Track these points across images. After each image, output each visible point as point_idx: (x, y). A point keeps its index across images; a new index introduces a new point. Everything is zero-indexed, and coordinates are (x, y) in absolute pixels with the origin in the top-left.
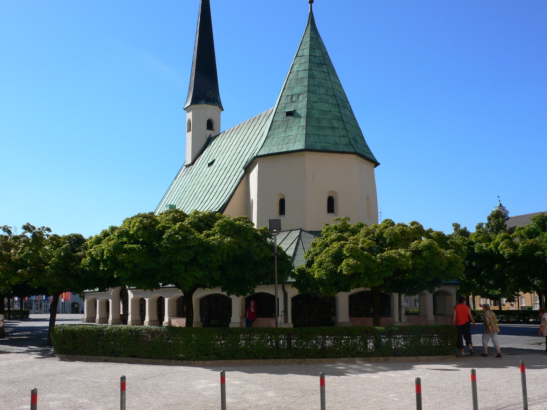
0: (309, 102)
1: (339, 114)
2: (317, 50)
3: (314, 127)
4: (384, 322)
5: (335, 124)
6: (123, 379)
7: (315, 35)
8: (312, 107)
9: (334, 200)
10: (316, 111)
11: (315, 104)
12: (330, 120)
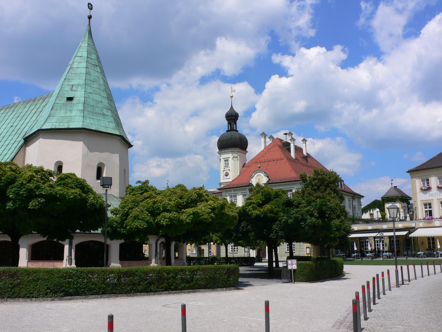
0: (86, 92)
3: (90, 112)
5: (105, 111)
6: (111, 318)
7: (92, 43)
8: (88, 96)
9: (101, 170)
11: (91, 94)
12: (101, 108)
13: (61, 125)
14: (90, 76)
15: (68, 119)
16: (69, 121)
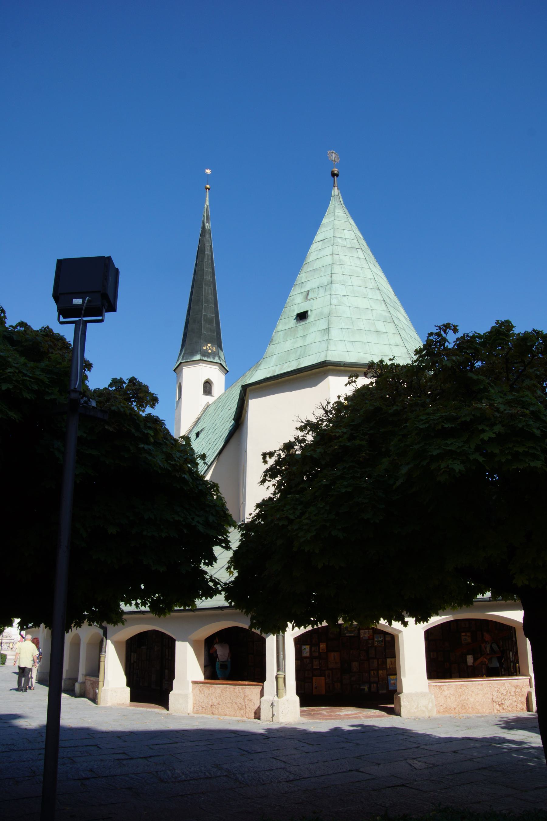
1: (387, 314)
5: (381, 326)
11: (345, 298)
12: (372, 321)
13: (284, 367)
14: (342, 266)
15: (298, 353)
16: (300, 356)
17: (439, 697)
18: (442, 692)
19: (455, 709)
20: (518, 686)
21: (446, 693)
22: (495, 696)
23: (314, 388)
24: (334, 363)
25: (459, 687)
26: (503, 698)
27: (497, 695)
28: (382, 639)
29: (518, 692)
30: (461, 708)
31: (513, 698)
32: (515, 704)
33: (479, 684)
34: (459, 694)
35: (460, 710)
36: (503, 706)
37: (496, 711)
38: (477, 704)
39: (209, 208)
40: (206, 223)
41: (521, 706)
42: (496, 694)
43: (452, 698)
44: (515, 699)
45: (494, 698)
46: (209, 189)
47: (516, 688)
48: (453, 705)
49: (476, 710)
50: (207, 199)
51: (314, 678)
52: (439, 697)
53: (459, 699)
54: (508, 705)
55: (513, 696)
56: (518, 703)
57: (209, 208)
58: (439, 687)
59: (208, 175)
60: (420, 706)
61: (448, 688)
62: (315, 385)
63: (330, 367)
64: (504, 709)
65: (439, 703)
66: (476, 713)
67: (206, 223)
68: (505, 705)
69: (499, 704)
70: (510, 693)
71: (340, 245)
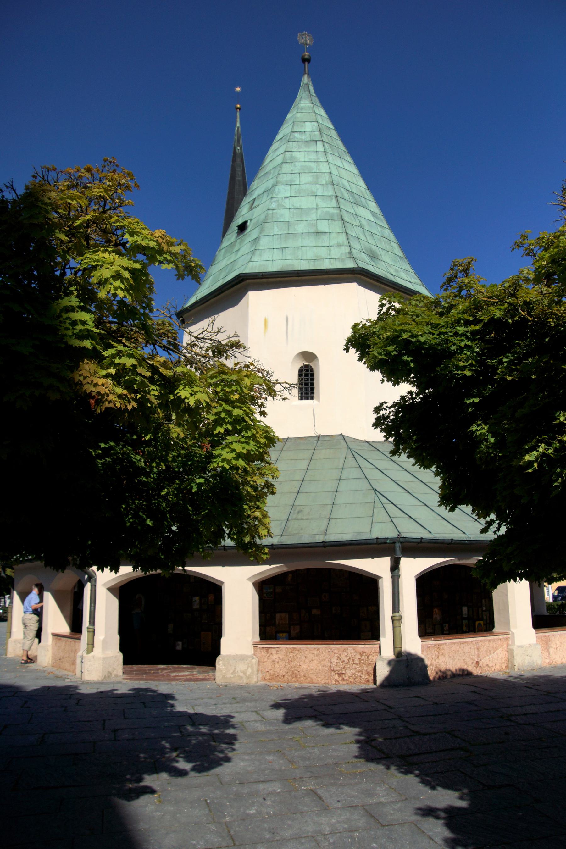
1: (336, 211)
2: (309, 123)
4: (350, 655)
7: (310, 104)
10: (286, 212)
11: (287, 200)
12: (314, 222)
17: (266, 661)
18: (269, 656)
19: (284, 676)
20: (364, 652)
21: (274, 657)
22: (334, 663)
23: (236, 307)
24: (250, 276)
25: (290, 650)
26: (344, 667)
27: (336, 663)
28: (271, 590)
29: (363, 659)
30: (292, 676)
31: (357, 667)
32: (359, 674)
33: (315, 648)
34: (290, 659)
35: (290, 678)
36: (344, 676)
37: (333, 682)
38: (311, 672)
39: (240, 129)
40: (237, 146)
41: (367, 677)
42: (335, 662)
43: (281, 663)
44: (360, 668)
45: (334, 665)
46: (240, 109)
47: (361, 655)
48: (281, 672)
49: (309, 679)
50: (238, 120)
51: (202, 633)
52: (266, 661)
53: (289, 666)
54: (350, 675)
55: (357, 664)
56: (362, 674)
57: (240, 129)
58: (267, 649)
59: (238, 93)
60: (238, 671)
61: (277, 651)
62: (236, 304)
63: (250, 281)
64: (344, 680)
65: (265, 669)
66: (309, 683)
67: (237, 146)
68: (346, 675)
69: (339, 674)
70: (353, 660)
71: (296, 140)
